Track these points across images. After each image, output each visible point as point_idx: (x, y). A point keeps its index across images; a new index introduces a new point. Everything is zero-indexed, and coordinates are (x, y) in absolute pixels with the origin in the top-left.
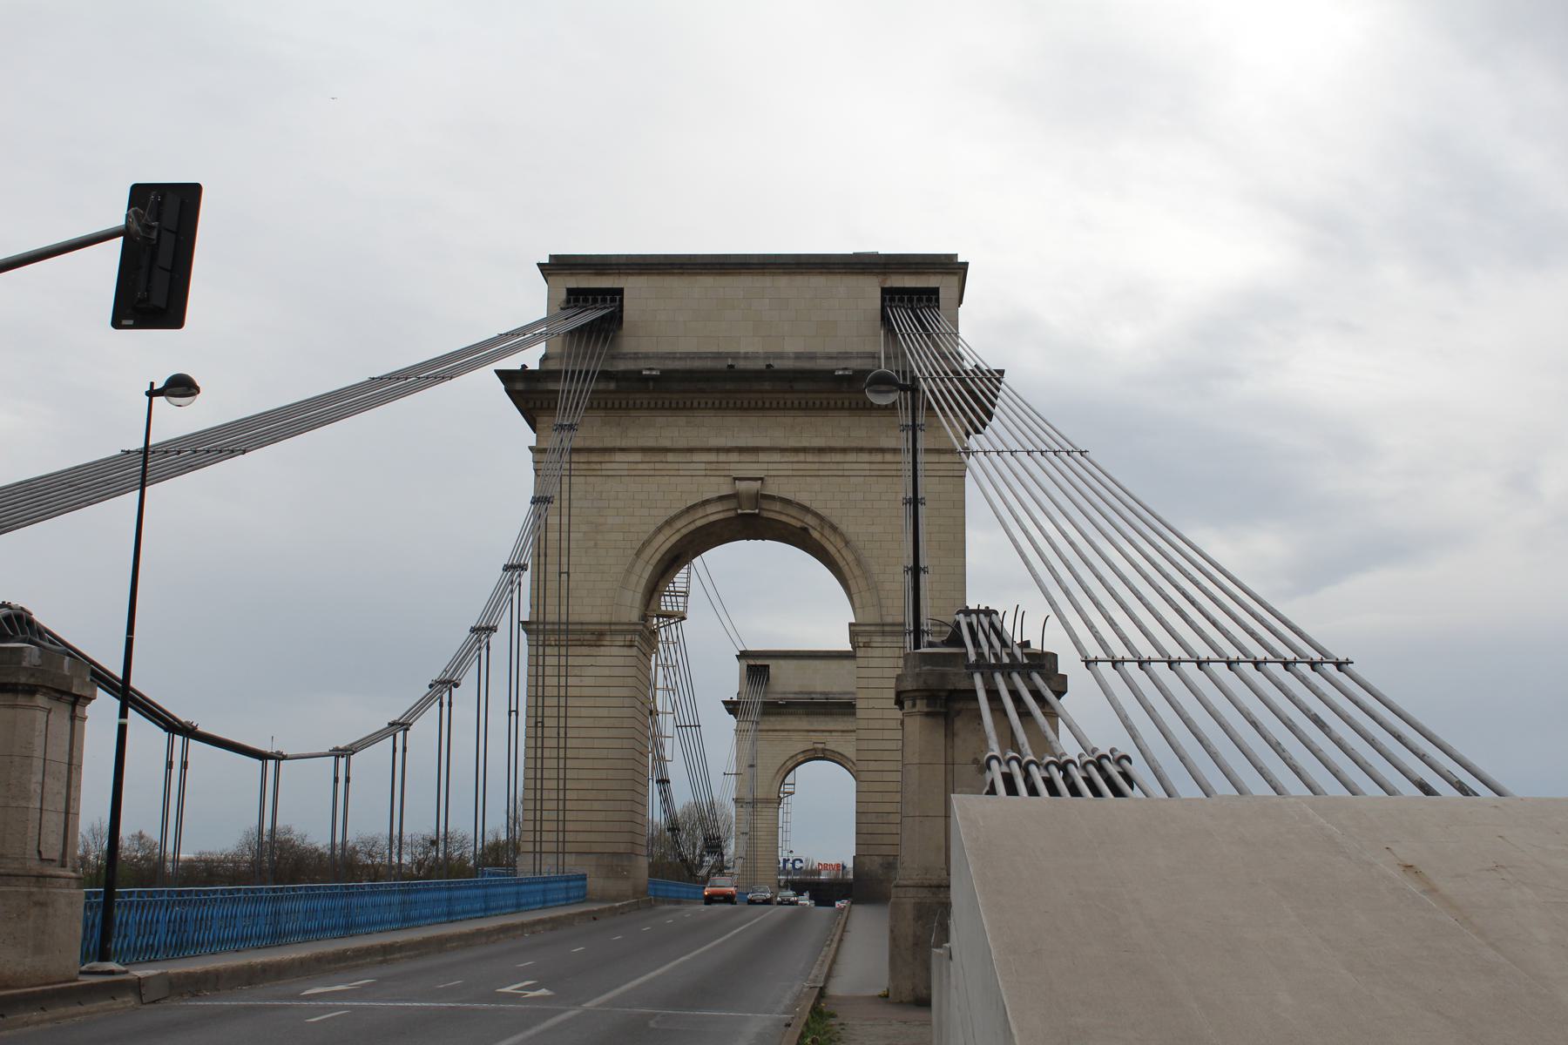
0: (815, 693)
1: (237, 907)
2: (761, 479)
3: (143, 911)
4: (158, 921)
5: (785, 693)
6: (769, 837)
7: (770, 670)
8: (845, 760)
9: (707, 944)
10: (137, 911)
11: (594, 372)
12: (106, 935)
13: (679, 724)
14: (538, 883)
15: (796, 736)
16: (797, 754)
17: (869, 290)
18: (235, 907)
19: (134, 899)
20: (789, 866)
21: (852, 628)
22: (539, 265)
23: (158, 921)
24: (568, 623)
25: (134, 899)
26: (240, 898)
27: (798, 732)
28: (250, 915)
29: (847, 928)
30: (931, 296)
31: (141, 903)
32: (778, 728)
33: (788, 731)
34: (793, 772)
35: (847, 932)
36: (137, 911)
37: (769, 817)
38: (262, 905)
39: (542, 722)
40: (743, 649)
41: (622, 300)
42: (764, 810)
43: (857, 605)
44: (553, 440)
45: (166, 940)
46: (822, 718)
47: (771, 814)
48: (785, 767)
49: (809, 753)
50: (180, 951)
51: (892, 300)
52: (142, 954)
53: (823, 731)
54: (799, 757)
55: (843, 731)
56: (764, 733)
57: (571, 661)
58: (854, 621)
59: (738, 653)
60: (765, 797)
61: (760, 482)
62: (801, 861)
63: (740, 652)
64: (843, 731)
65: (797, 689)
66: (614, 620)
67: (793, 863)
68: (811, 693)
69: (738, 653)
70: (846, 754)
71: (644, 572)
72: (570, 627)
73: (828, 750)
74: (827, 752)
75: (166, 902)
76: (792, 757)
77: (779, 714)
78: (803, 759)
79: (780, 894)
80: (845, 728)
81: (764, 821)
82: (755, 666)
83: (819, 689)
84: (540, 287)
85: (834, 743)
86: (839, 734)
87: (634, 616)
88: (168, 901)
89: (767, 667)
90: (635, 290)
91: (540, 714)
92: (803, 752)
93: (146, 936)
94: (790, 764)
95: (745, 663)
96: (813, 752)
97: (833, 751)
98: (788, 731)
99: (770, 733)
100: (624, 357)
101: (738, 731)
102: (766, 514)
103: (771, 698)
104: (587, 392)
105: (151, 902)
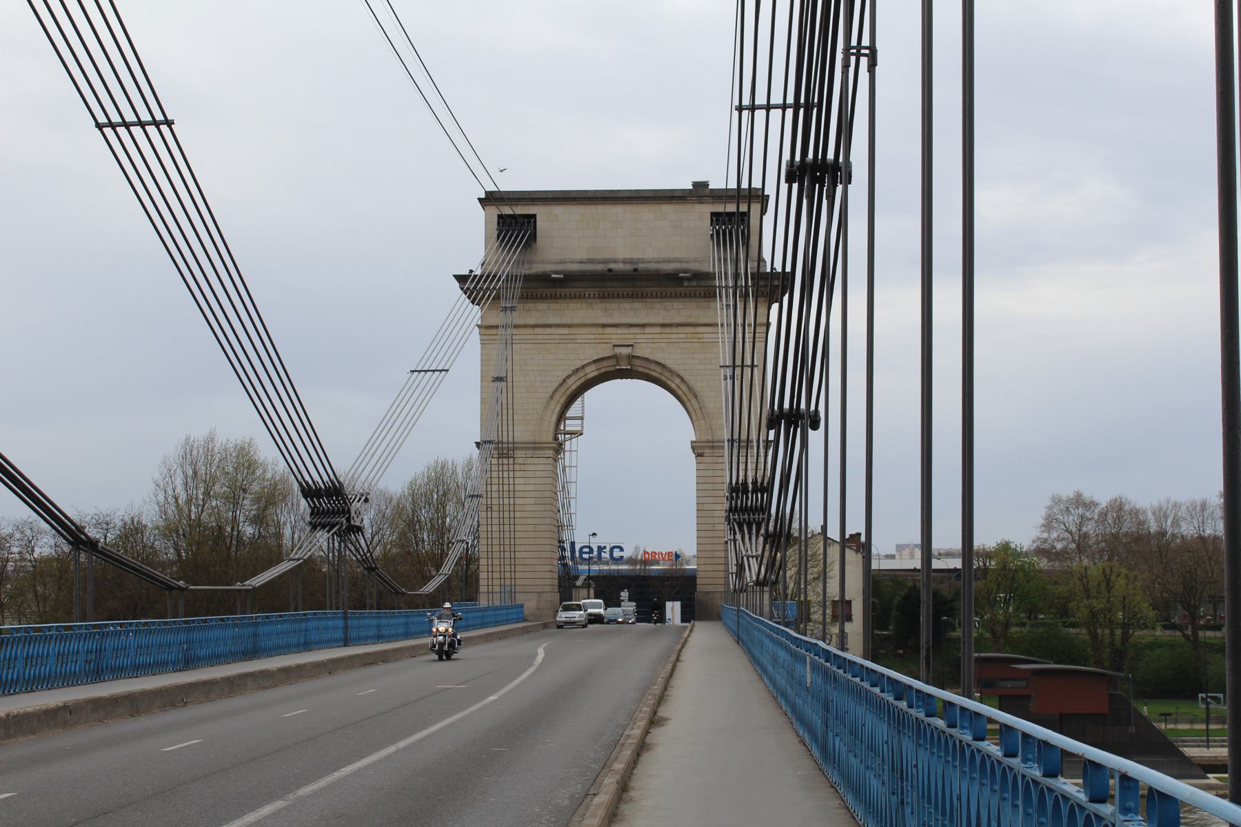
0: (615, 261)
1: (17, 647)
2: (632, 345)
3: (12, 647)
6: (541, 508)
7: (538, 224)
8: (667, 374)
10: (56, 642)
11: (521, 276)
12: (426, 632)
14: (514, 608)
17: (701, 214)
18: (47, 645)
21: (693, 444)
22: (479, 199)
24: (514, 443)
25: (53, 632)
26: (195, 627)
28: (122, 648)
29: (682, 658)
30: (744, 217)
33: (569, 326)
35: (681, 661)
36: (56, 642)
39: (491, 508)
40: (494, 189)
41: (535, 222)
42: (529, 461)
43: (694, 418)
44: (496, 318)
45: (56, 669)
46: (626, 305)
47: (542, 467)
49: (605, 364)
50: (11, 687)
51: (718, 220)
52: (46, 683)
53: (631, 326)
54: (588, 369)
55: (663, 325)
56: (530, 331)
58: (695, 440)
59: (483, 196)
60: (531, 439)
61: (631, 347)
63: (486, 193)
64: (663, 325)
65: (585, 257)
66: (537, 440)
68: (606, 262)
69: (483, 196)
70: (668, 363)
72: (515, 445)
73: (638, 357)
74: (637, 362)
75: (84, 635)
76: (577, 370)
77: (554, 298)
78: (596, 373)
80: (668, 321)
83: (621, 255)
84: (479, 214)
85: (649, 347)
86: (658, 330)
88: (86, 634)
91: (489, 503)
94: (573, 383)
95: (494, 211)
96: (613, 362)
97: (646, 359)
99: (539, 331)
100: (542, 262)
101: (485, 328)
102: (635, 368)
103: (538, 268)
104: (518, 288)
105: (26, 638)
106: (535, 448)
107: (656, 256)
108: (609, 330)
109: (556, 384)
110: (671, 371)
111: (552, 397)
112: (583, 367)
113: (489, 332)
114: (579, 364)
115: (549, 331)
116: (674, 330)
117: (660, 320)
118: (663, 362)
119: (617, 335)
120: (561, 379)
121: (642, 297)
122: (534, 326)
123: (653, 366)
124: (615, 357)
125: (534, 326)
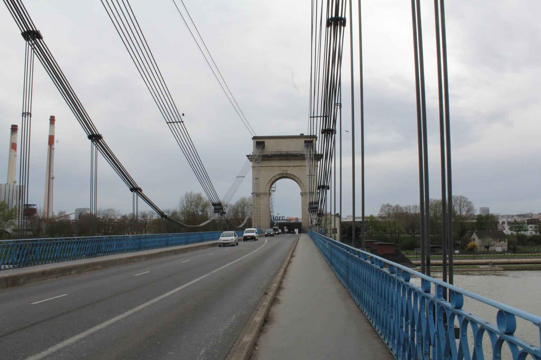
0: (283, 152)
4: (124, 244)
7: (265, 143)
9: (149, 300)
13: (181, 123)
15: (275, 168)
16: (276, 176)
17: (302, 141)
19: (157, 236)
20: (281, 218)
23: (124, 244)
27: (276, 167)
31: (100, 240)
32: (269, 165)
34: (275, 183)
40: (255, 136)
44: (256, 165)
46: (285, 161)
48: (272, 180)
49: (280, 175)
51: (306, 142)
54: (277, 176)
59: (253, 137)
62: (284, 217)
64: (294, 166)
65: (276, 151)
67: (282, 217)
68: (281, 152)
69: (253, 137)
71: (271, 183)
73: (288, 174)
79: (267, 230)
83: (284, 150)
84: (252, 141)
85: (290, 171)
86: (292, 167)
89: (263, 142)
90: (267, 142)
92: (278, 174)
93: (110, 248)
94: (273, 179)
95: (255, 141)
96: (282, 174)
97: (290, 174)
103: (265, 153)
106: (265, 194)
107: (292, 150)
108: (281, 167)
109: (269, 180)
115: (267, 168)
116: (296, 167)
117: (293, 165)
120: (270, 179)
122: (264, 167)
124: (283, 174)
125: (264, 167)
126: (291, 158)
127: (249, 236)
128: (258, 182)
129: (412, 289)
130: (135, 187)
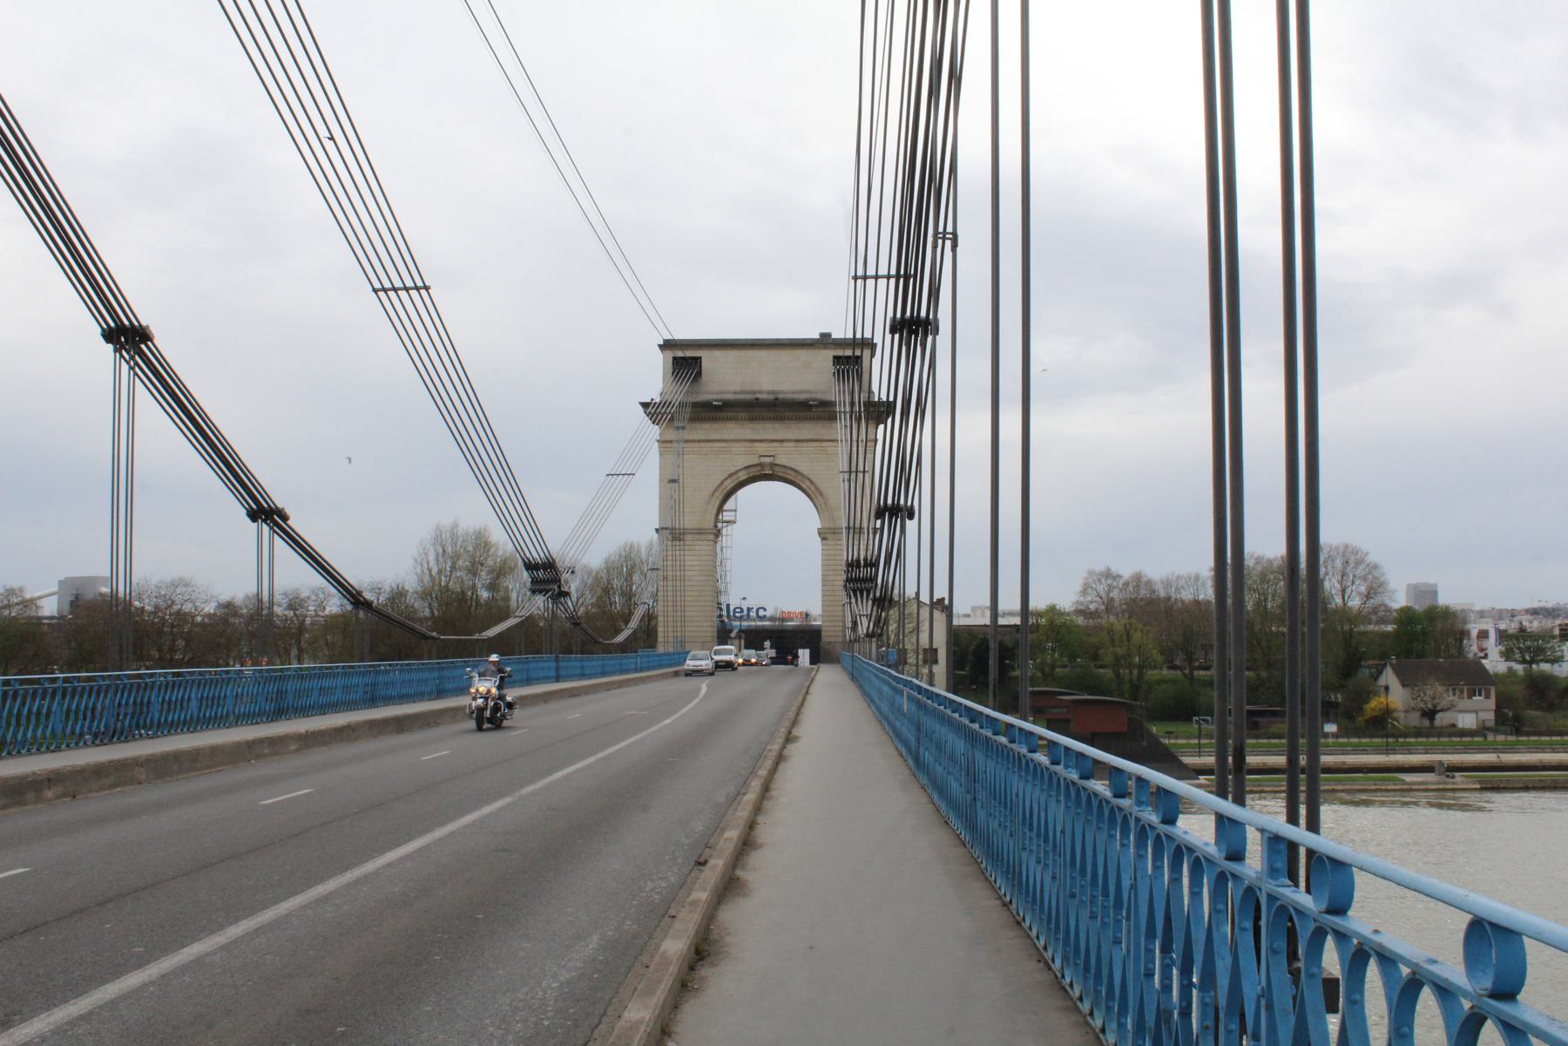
4: (312, 689)
5: (722, 393)
6: (704, 578)
8: (799, 477)
15: (737, 447)
24: (684, 529)
33: (726, 441)
37: (703, 553)
38: (316, 680)
41: (701, 362)
42: (696, 543)
44: (671, 435)
49: (752, 469)
53: (773, 441)
54: (740, 474)
57: (687, 553)
65: (738, 388)
66: (702, 527)
73: (777, 465)
77: (715, 419)
80: (801, 437)
81: (697, 558)
82: (684, 358)
85: (786, 456)
86: (793, 444)
87: (711, 525)
89: (697, 360)
90: (708, 358)
94: (729, 484)
95: (670, 355)
96: (758, 468)
97: (784, 466)
98: (726, 441)
99: (702, 444)
101: (663, 442)
106: (700, 533)
107: (792, 388)
108: (756, 444)
109: (716, 485)
110: (803, 476)
111: (713, 495)
112: (737, 472)
113: (665, 445)
114: (733, 469)
118: (796, 468)
119: (761, 448)
120: (719, 482)
121: (781, 419)
123: (789, 472)
124: (761, 465)
126: (787, 414)
127: (595, 678)
128: (677, 493)
129: (1184, 849)
130: (265, 505)
